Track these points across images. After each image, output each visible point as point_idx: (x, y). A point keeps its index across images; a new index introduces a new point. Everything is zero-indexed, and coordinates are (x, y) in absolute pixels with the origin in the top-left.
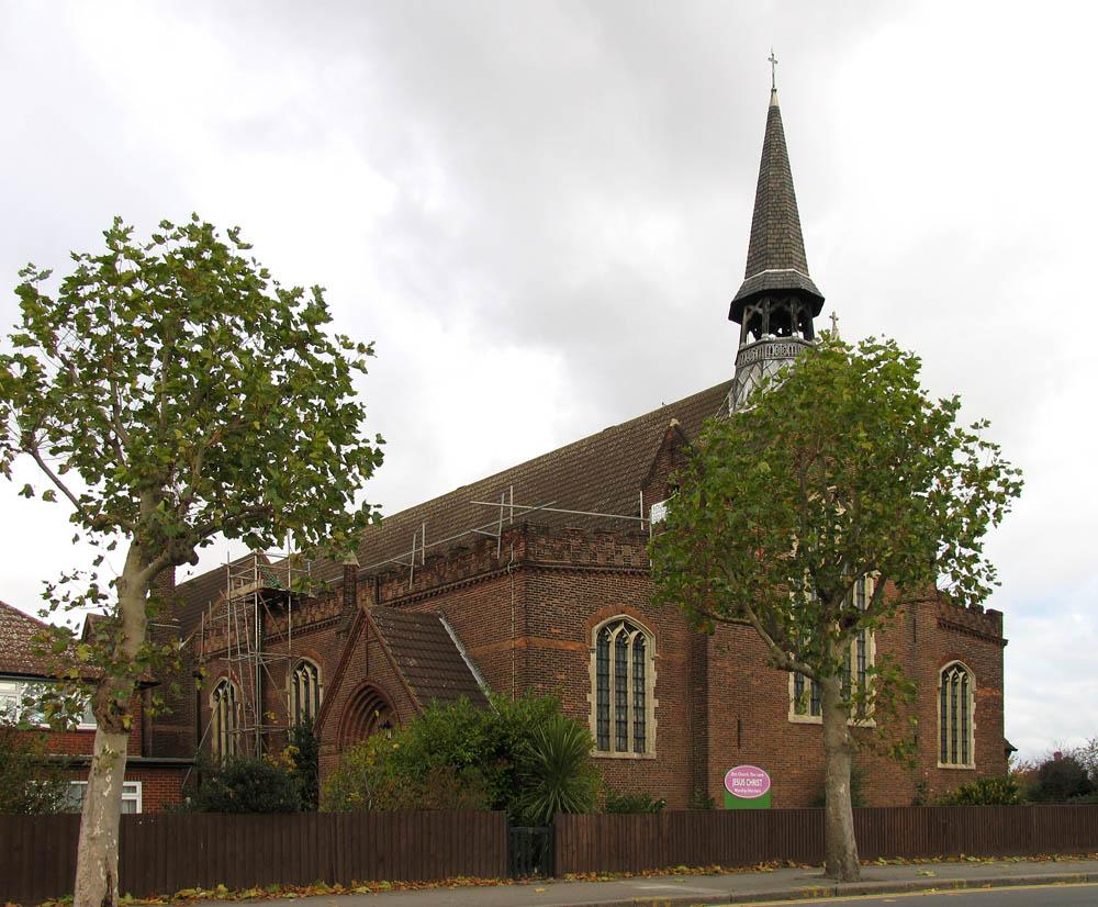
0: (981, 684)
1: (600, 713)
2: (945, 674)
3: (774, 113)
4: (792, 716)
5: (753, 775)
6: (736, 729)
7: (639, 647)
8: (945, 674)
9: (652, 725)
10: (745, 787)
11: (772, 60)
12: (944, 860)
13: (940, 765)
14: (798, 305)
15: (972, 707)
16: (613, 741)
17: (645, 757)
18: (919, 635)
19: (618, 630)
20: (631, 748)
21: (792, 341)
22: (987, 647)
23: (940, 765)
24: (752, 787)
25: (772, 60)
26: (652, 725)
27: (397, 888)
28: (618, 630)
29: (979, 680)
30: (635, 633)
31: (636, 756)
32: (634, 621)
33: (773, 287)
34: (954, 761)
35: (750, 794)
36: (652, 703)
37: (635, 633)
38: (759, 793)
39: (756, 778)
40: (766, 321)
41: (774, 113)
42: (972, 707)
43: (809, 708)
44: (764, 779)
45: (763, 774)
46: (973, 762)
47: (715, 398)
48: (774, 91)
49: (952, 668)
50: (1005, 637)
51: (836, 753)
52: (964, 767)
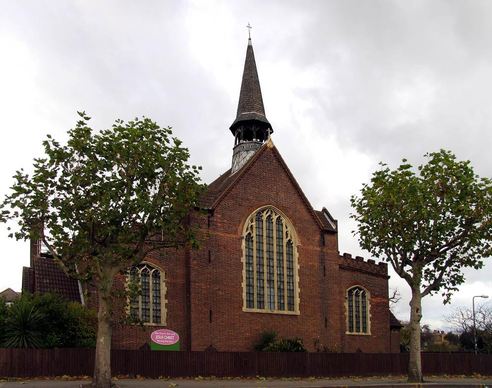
0: (373, 295)
1: (350, 319)
2: (350, 292)
3: (250, 48)
4: (245, 309)
5: (168, 334)
6: (209, 314)
7: (364, 296)
8: (350, 292)
9: (164, 311)
10: (164, 339)
11: (249, 27)
12: (348, 377)
13: (348, 333)
14: (257, 128)
15: (369, 307)
16: (361, 329)
17: (159, 325)
18: (327, 273)
19: (355, 291)
20: (354, 331)
21: (252, 143)
22: (378, 280)
23: (348, 333)
24: (167, 340)
25: (249, 27)
26: (164, 311)
27: (232, 379)
28: (355, 291)
29: (371, 294)
30: (362, 291)
31: (154, 324)
32: (152, 265)
33: (243, 120)
34: (358, 331)
35: (162, 343)
36: (164, 301)
37: (362, 291)
38: (172, 342)
39: (171, 335)
40: (242, 134)
41: (250, 48)
42: (369, 307)
43: (256, 303)
44: (175, 337)
45: (175, 334)
46: (369, 332)
47: (229, 172)
48: (250, 39)
49: (355, 288)
50: (389, 275)
51: (101, 321)
52: (364, 334)
